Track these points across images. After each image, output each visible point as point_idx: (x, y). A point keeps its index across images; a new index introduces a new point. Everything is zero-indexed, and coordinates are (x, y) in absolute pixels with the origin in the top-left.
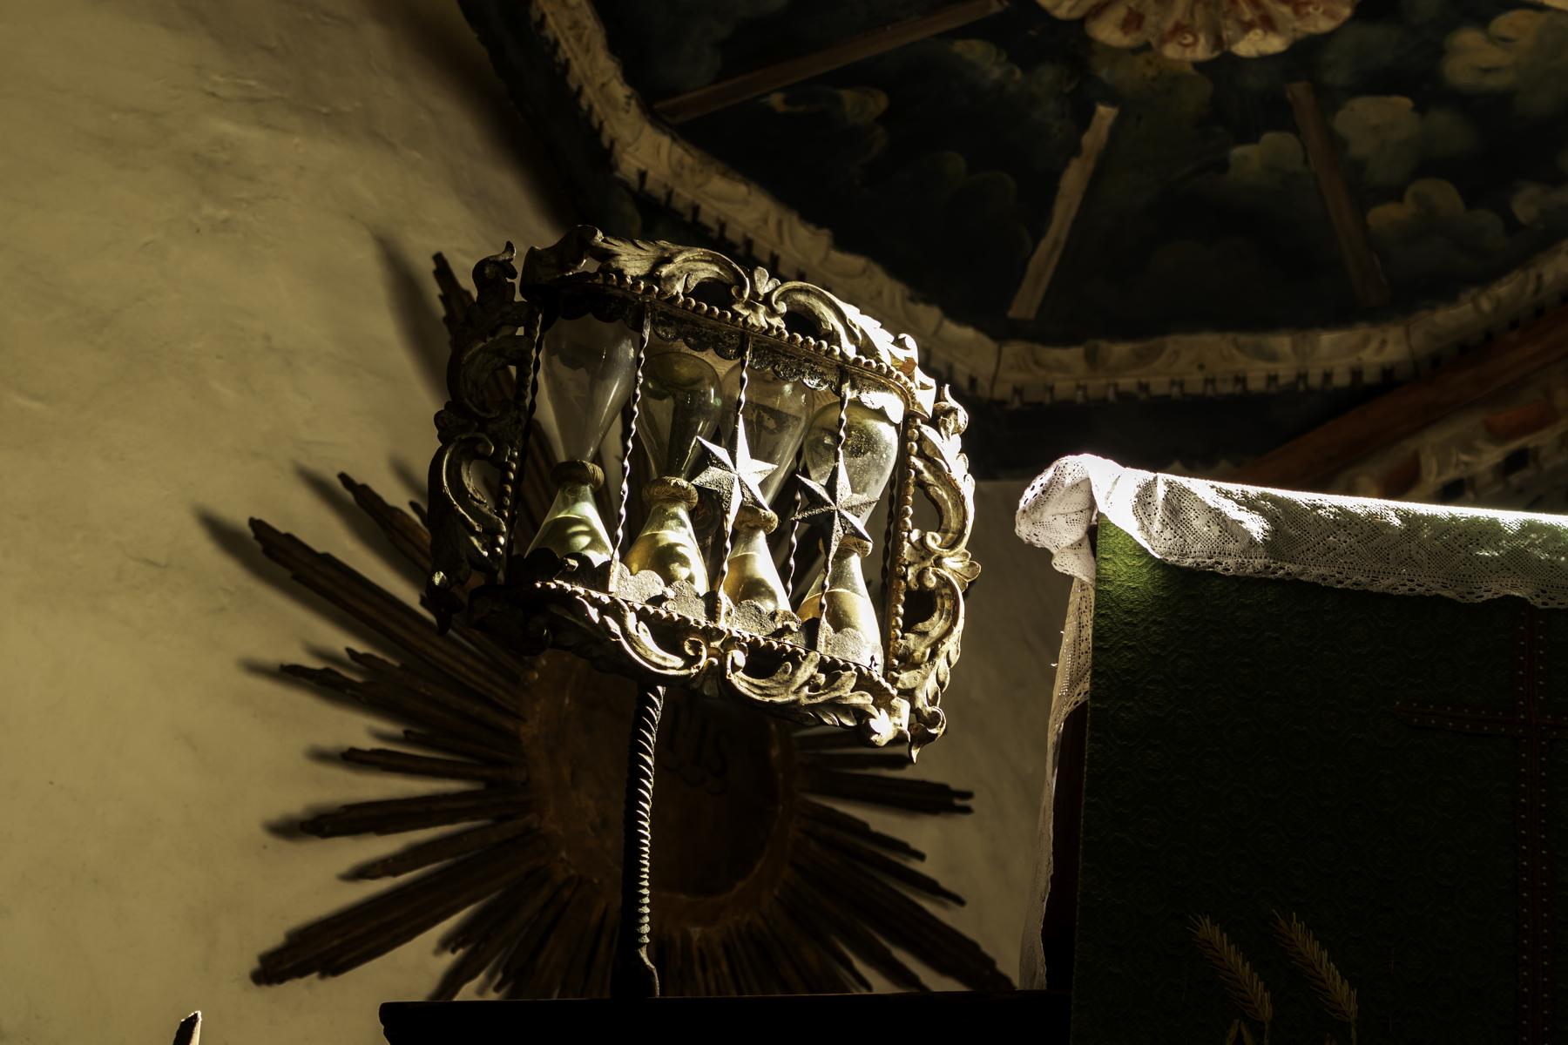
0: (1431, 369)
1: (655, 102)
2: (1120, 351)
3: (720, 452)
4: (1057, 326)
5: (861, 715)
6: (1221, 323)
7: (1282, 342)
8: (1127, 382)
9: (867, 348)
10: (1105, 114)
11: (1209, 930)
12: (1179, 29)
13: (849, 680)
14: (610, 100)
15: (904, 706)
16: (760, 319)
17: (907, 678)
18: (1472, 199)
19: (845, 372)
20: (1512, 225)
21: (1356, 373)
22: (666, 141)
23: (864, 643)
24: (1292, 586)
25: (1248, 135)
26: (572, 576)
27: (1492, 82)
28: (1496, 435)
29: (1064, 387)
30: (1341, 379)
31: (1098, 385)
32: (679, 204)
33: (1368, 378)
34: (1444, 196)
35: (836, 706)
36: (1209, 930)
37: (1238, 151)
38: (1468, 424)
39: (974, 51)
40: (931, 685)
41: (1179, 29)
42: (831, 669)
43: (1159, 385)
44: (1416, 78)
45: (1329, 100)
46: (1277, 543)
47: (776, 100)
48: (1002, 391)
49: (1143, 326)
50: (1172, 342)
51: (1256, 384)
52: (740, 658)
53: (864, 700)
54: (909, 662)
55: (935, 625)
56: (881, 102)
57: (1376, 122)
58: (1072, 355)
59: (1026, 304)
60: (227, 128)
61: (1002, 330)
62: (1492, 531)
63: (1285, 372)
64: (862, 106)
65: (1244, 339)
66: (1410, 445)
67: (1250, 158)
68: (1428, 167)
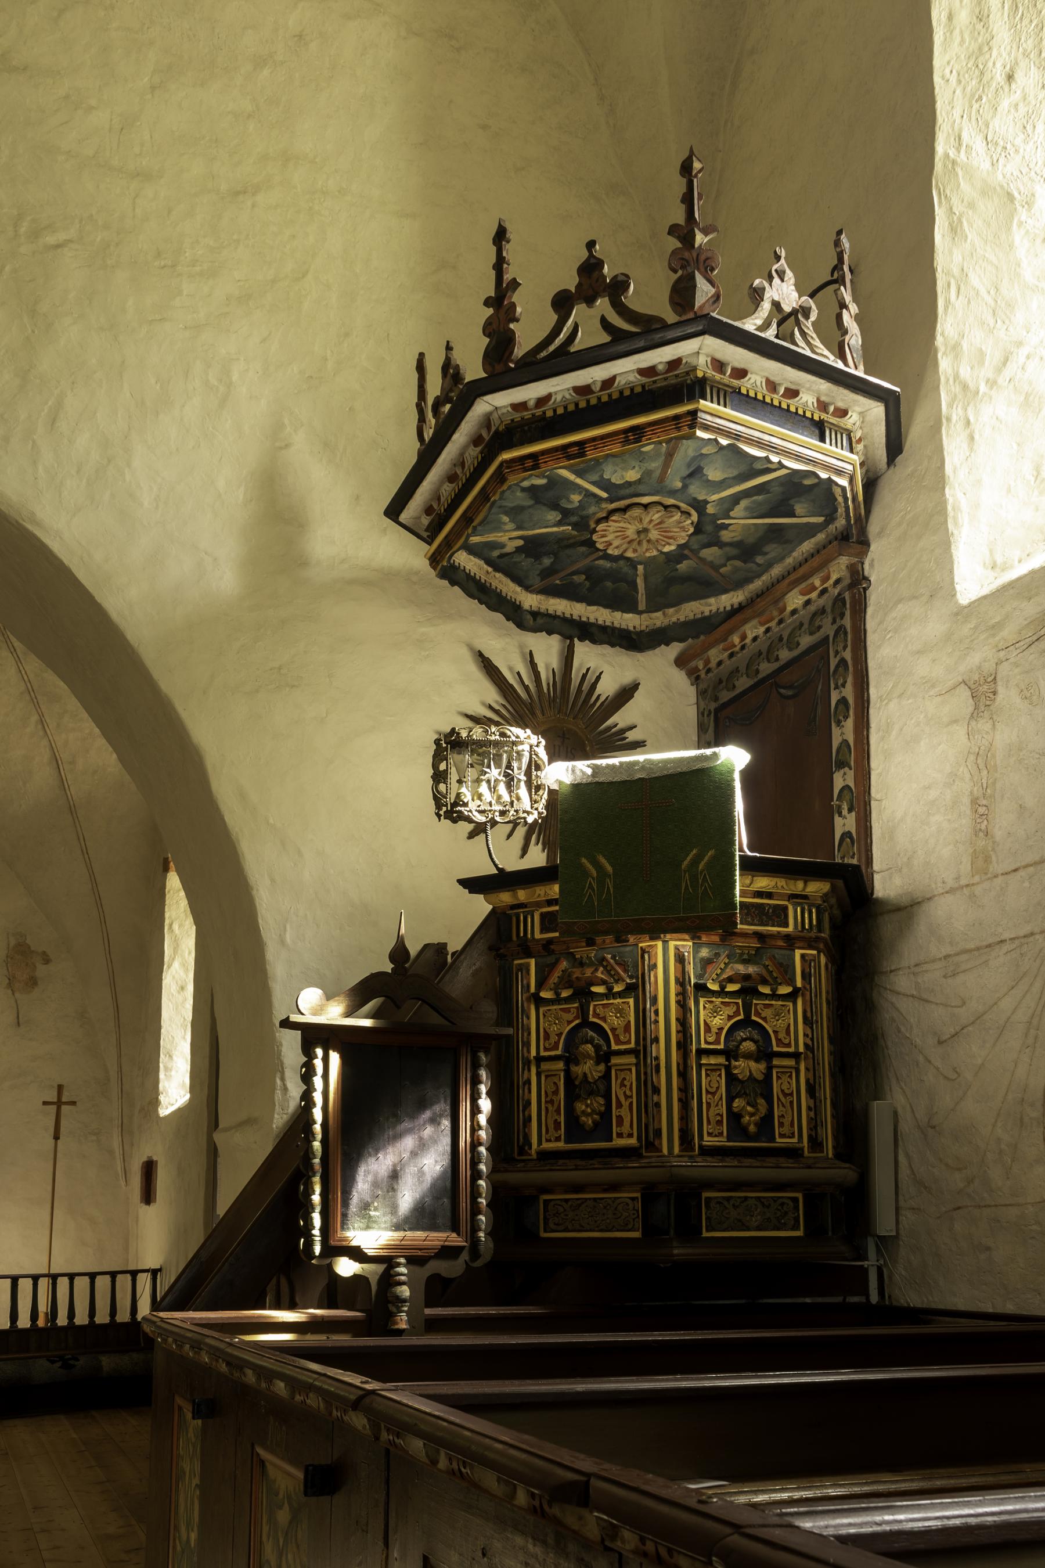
0: (751, 602)
1: (528, 588)
2: (671, 610)
3: (488, 770)
4: (650, 610)
5: (525, 818)
6: (695, 599)
7: (712, 600)
8: (674, 619)
9: (517, 737)
10: (640, 568)
11: (584, 860)
12: (647, 550)
13: (521, 812)
14: (516, 593)
15: (536, 812)
16: (493, 738)
17: (536, 806)
18: (745, 562)
19: (514, 743)
20: (759, 565)
21: (732, 606)
22: (534, 596)
23: (526, 803)
24: (597, 783)
25: (680, 562)
26: (461, 806)
27: (735, 539)
28: (762, 624)
29: (658, 624)
30: (729, 608)
31: (666, 622)
32: (542, 611)
33: (735, 607)
34: (738, 563)
35: (519, 818)
36: (584, 860)
37: (678, 566)
38: (755, 622)
39: (601, 562)
40: (541, 806)
41: (647, 550)
42: (517, 811)
43: (682, 619)
44: (718, 543)
45: (695, 552)
46: (594, 775)
47: (558, 582)
48: (643, 628)
49: (677, 603)
50: (683, 606)
51: (707, 613)
52: (497, 814)
53: (525, 815)
54: (536, 802)
55: (541, 792)
56: (584, 577)
57: (710, 553)
58: (659, 614)
59: (642, 606)
60: (423, 629)
61: (640, 613)
62: (636, 763)
63: (714, 609)
64: (580, 579)
65: (702, 601)
66: (743, 628)
67: (683, 567)
68: (729, 559)
